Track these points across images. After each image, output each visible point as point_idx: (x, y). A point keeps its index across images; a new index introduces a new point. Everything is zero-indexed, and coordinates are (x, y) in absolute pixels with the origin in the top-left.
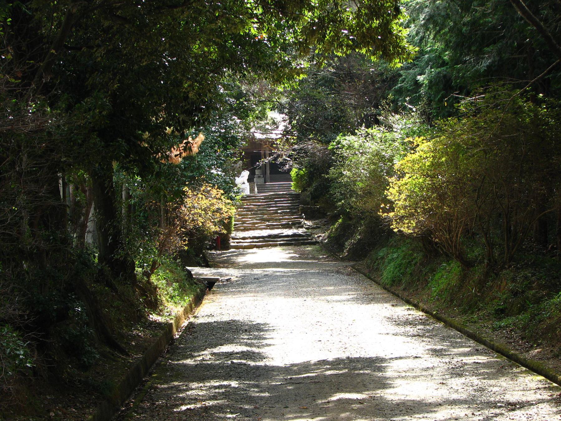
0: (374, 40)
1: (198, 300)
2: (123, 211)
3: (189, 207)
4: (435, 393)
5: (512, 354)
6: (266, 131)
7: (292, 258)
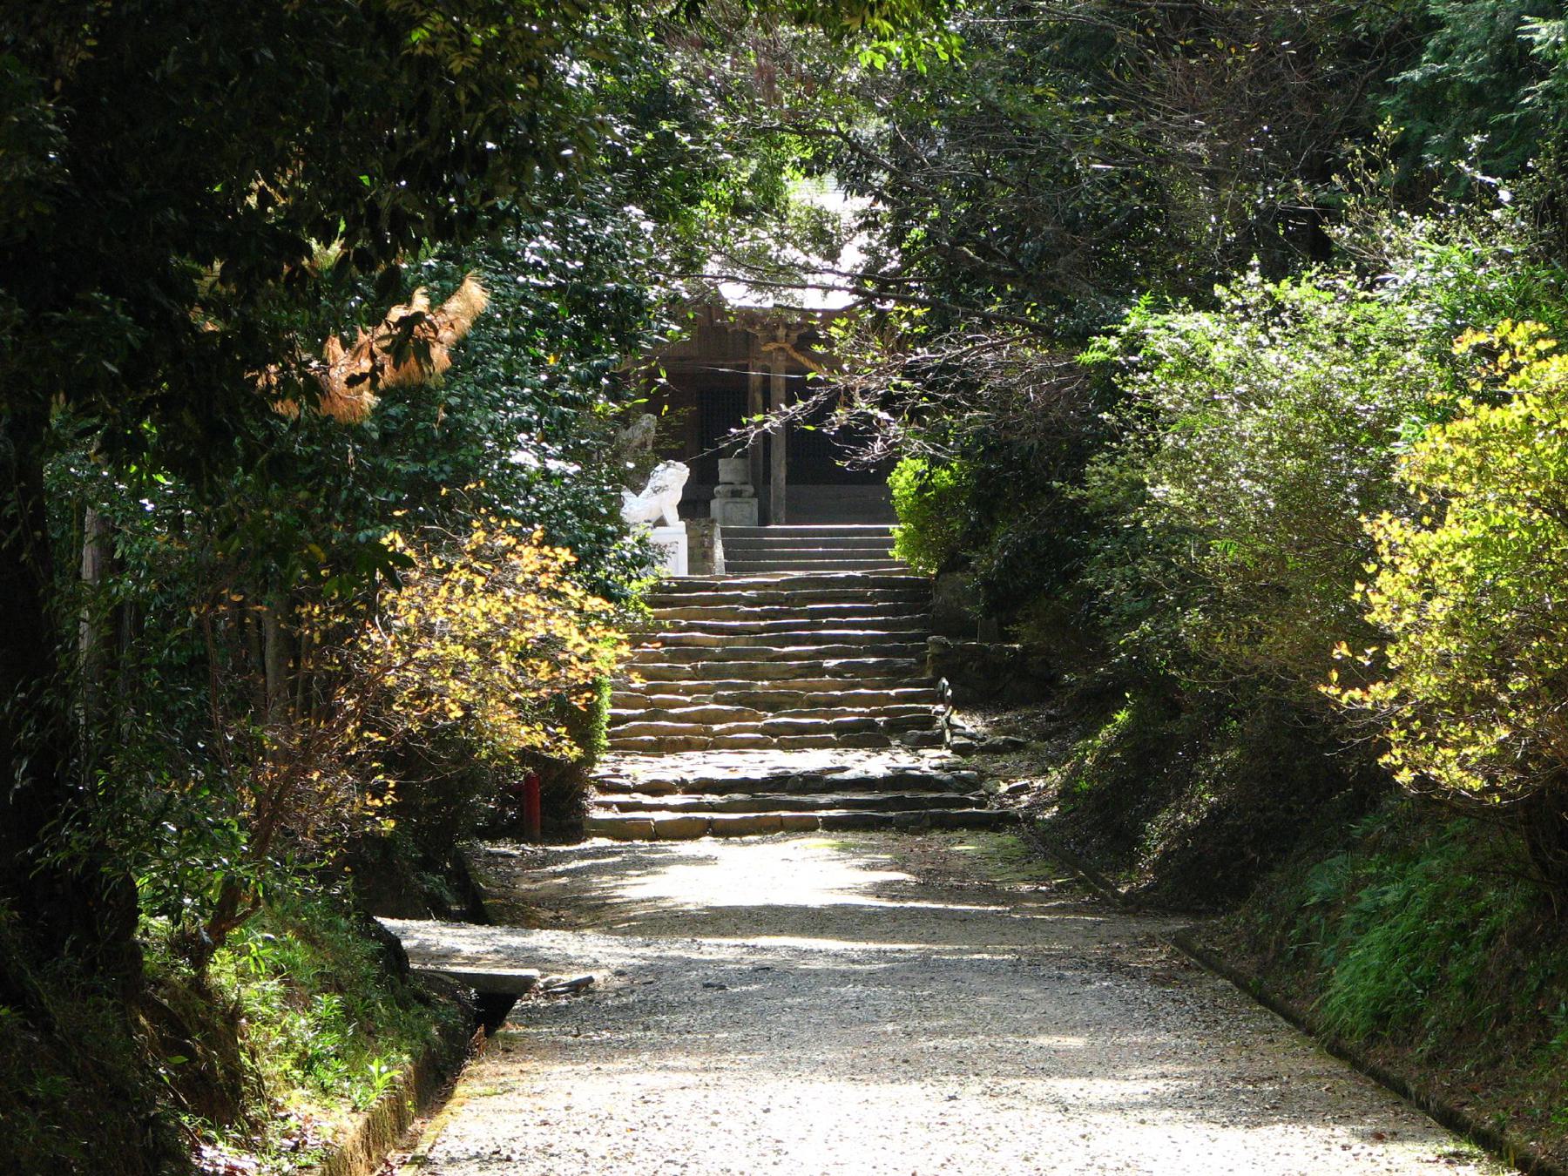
1: (434, 1082)
2: (83, 645)
3: (406, 630)
6: (770, 274)
7: (880, 890)
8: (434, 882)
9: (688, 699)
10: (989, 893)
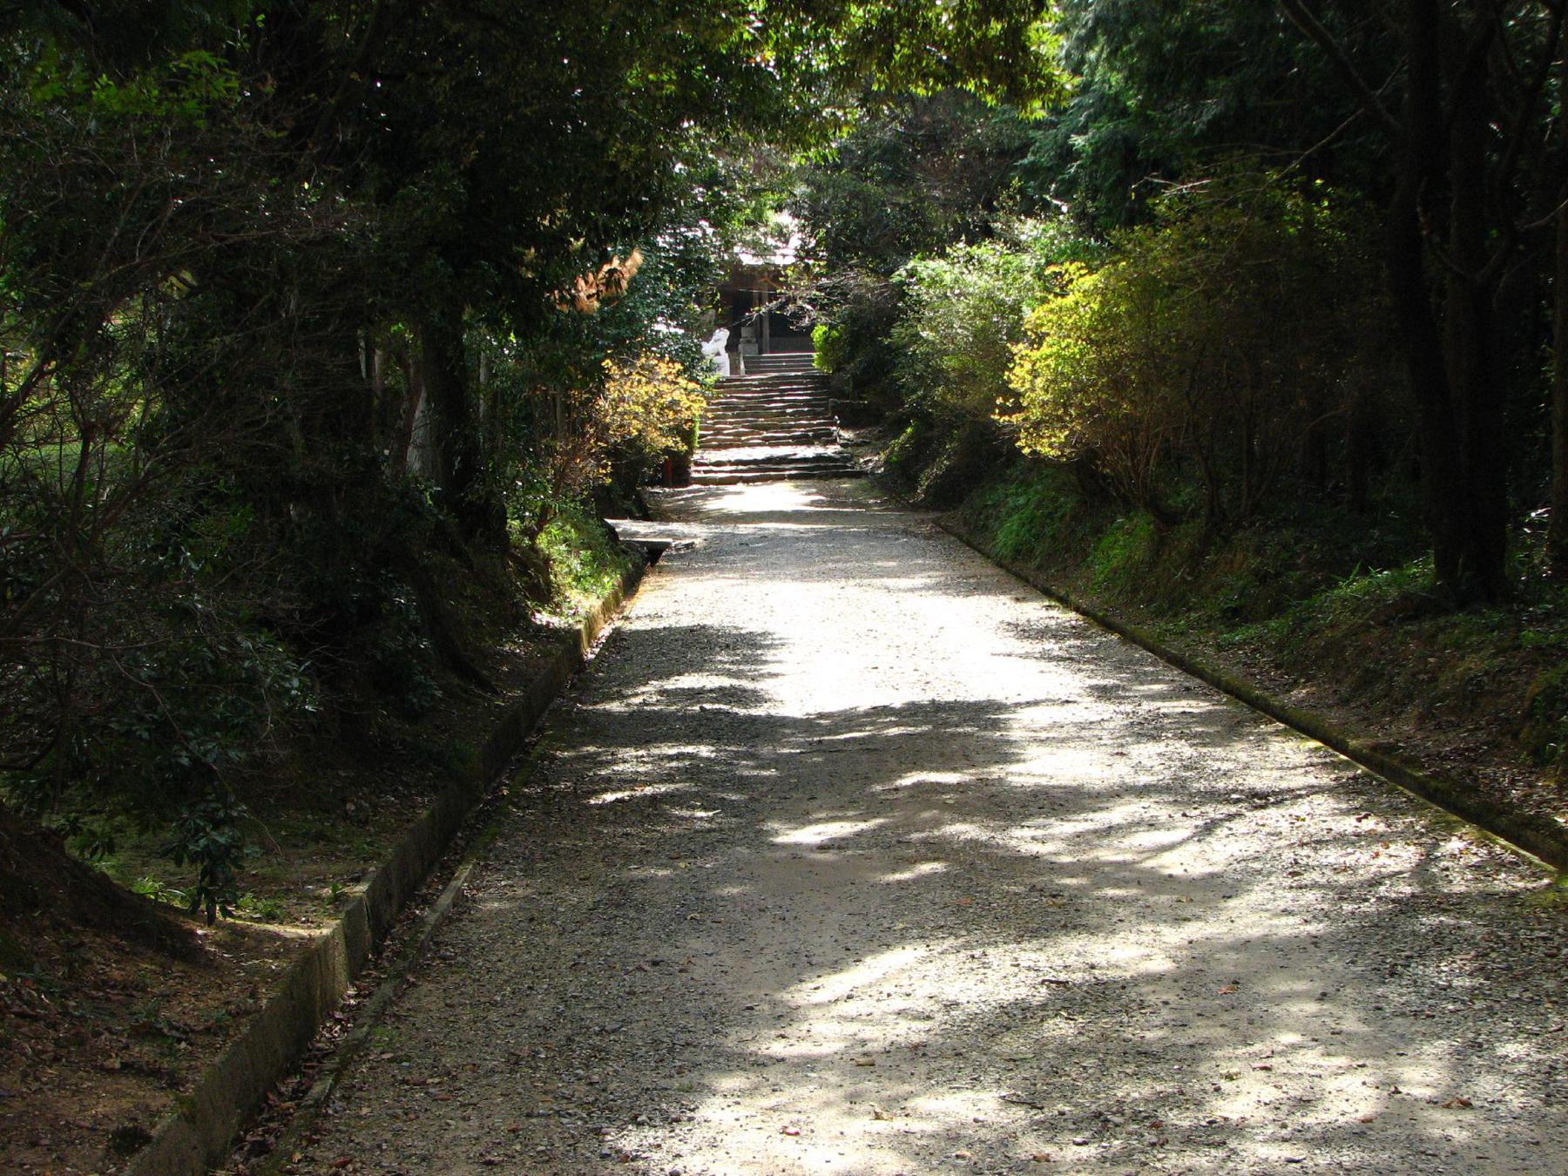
0: (992, 65)
1: (630, 586)
4: (1107, 772)
5: (1257, 697)
6: (760, 249)
7: (813, 503)
8: (628, 504)
10: (856, 504)
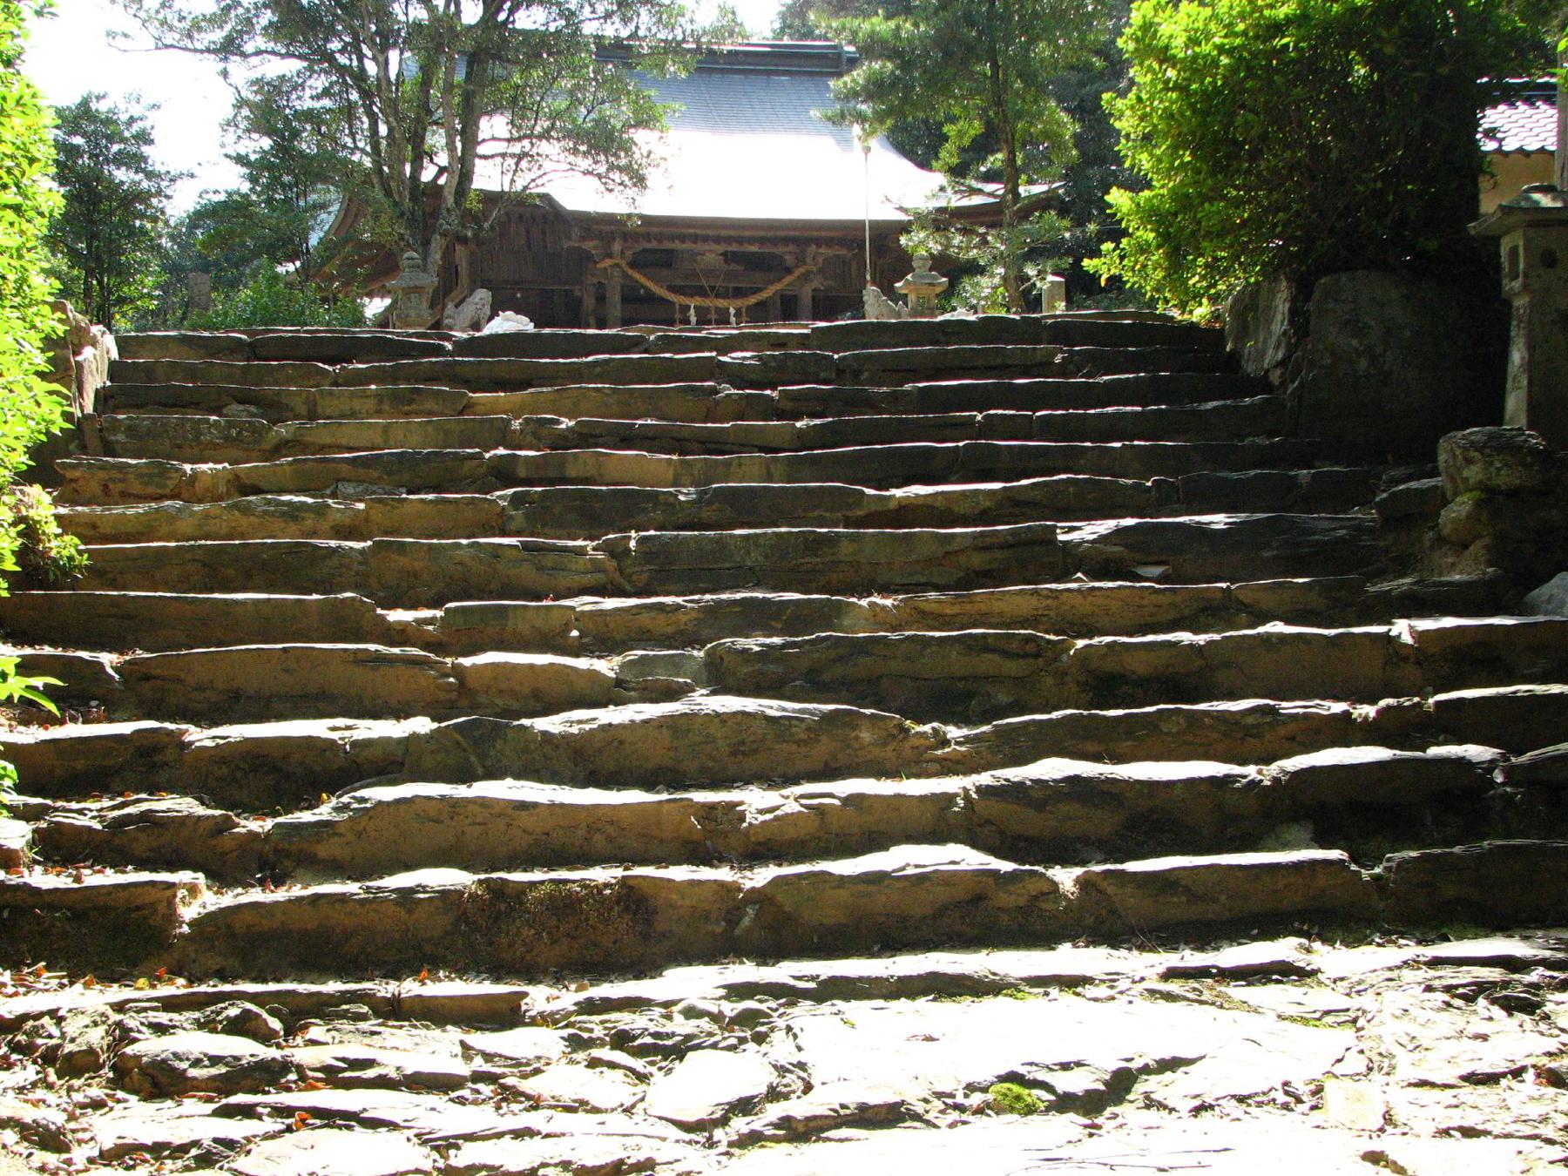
9: (606, 667)
